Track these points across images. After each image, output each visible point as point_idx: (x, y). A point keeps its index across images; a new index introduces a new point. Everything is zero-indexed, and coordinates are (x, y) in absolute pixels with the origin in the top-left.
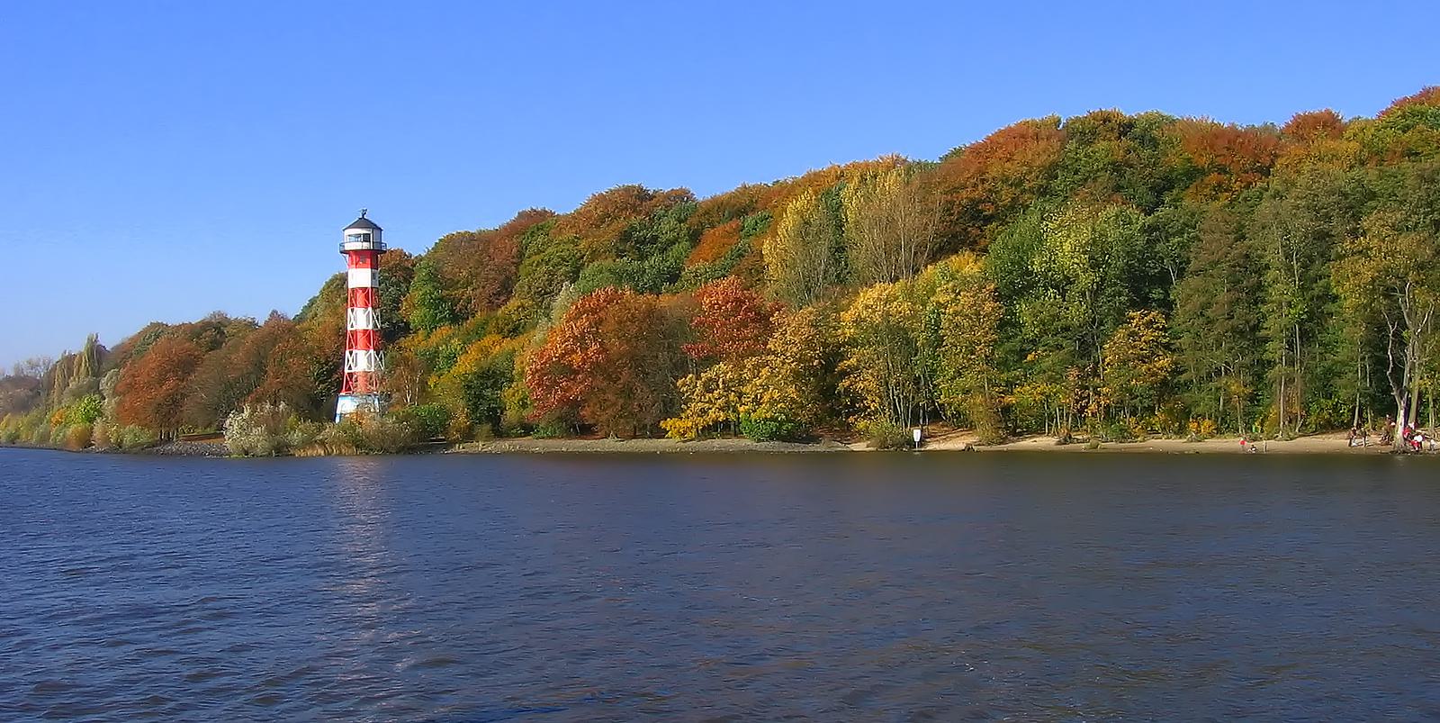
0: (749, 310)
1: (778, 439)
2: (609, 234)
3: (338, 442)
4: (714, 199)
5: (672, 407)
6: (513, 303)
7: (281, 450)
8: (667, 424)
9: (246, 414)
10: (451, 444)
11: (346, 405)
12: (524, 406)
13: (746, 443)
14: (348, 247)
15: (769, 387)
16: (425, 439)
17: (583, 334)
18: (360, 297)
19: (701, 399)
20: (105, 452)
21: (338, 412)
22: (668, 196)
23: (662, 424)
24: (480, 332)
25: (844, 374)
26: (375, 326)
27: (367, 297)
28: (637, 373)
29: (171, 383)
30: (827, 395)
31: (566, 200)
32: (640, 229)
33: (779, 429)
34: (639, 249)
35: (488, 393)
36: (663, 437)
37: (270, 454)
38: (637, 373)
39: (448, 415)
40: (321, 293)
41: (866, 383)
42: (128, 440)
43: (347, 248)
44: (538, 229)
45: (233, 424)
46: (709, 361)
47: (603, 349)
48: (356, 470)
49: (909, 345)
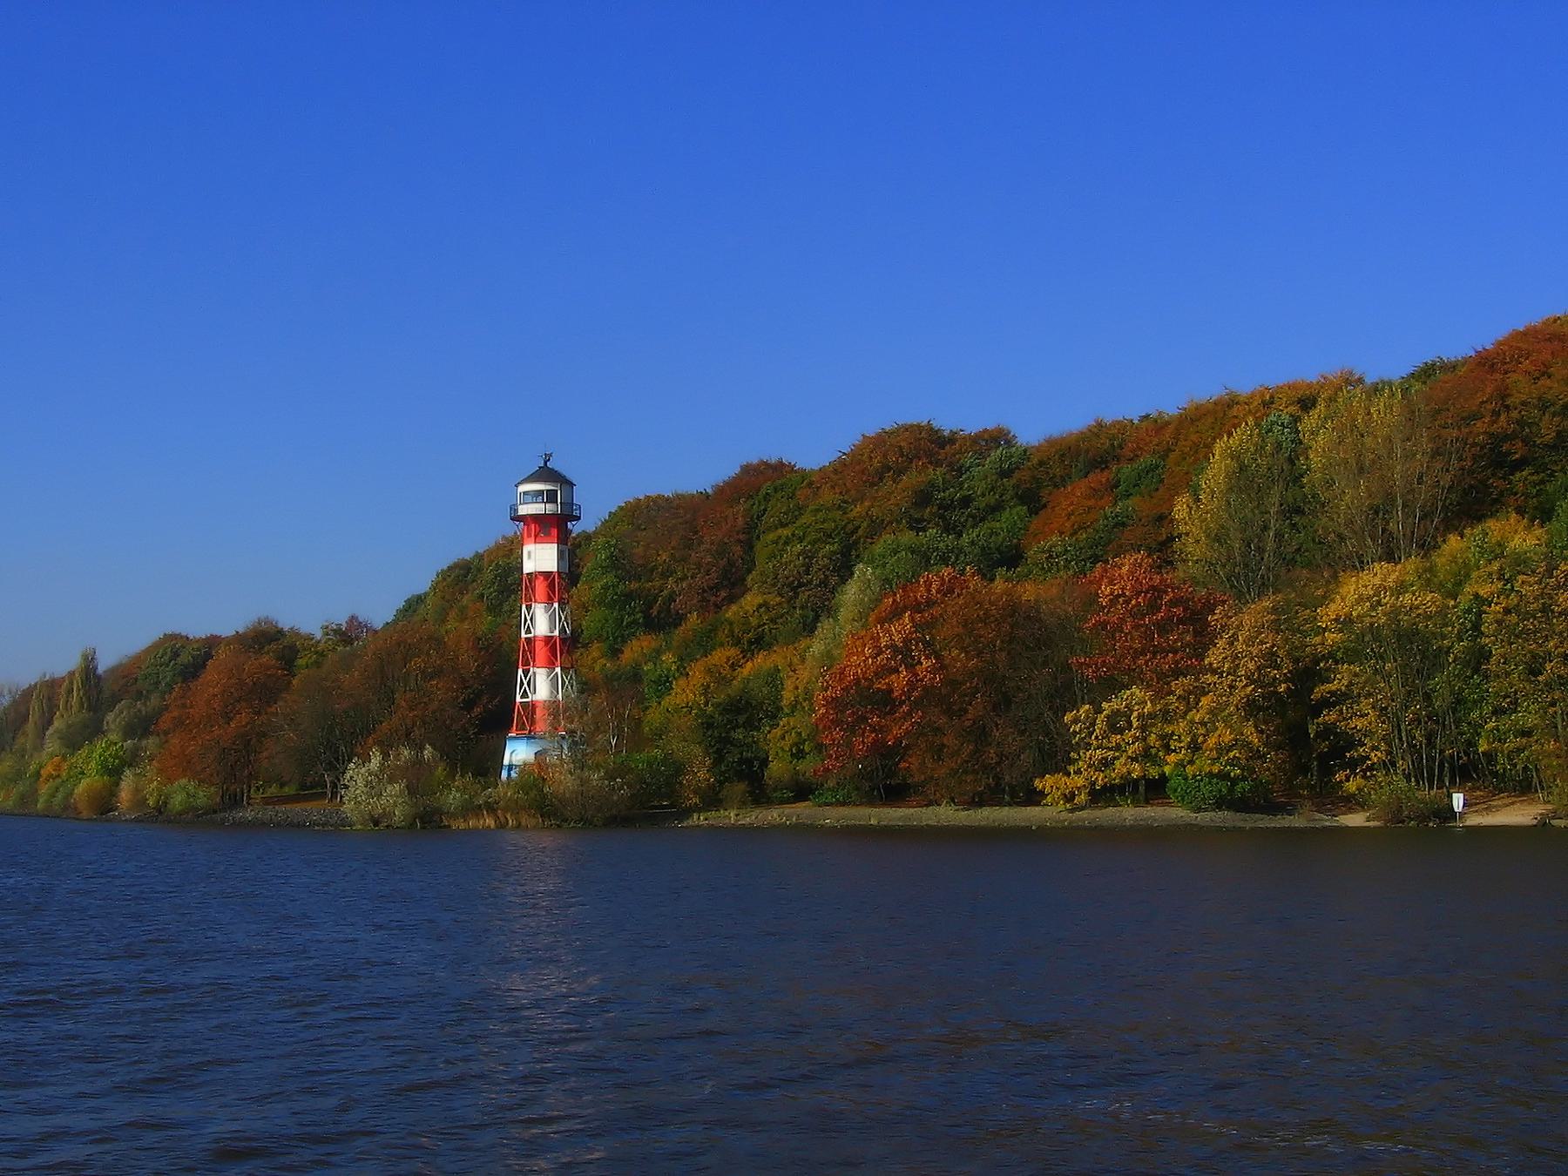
0: (1174, 603)
1: (1228, 808)
2: (897, 494)
3: (516, 808)
4: (1051, 442)
5: (1056, 758)
6: (750, 601)
7: (428, 820)
8: (1046, 783)
9: (375, 762)
10: (687, 813)
11: (518, 752)
12: (799, 754)
13: (1176, 813)
14: (524, 510)
15: (1213, 727)
16: (647, 805)
17: (906, 641)
18: (541, 587)
19: (1107, 737)
20: (137, 820)
21: (506, 762)
22: (975, 439)
23: (1038, 784)
24: (704, 642)
25: (1326, 703)
26: (563, 630)
27: (551, 586)
28: (996, 706)
29: (244, 717)
30: (1301, 738)
31: (814, 446)
32: (935, 486)
33: (1231, 790)
34: (942, 517)
35: (739, 735)
36: (1038, 804)
37: (412, 825)
38: (996, 706)
39: (679, 769)
40: (434, 588)
41: (1363, 720)
42: (177, 801)
43: (521, 513)
44: (776, 490)
45: (357, 776)
46: (1112, 686)
47: (941, 667)
48: (538, 845)
49: (1434, 661)
